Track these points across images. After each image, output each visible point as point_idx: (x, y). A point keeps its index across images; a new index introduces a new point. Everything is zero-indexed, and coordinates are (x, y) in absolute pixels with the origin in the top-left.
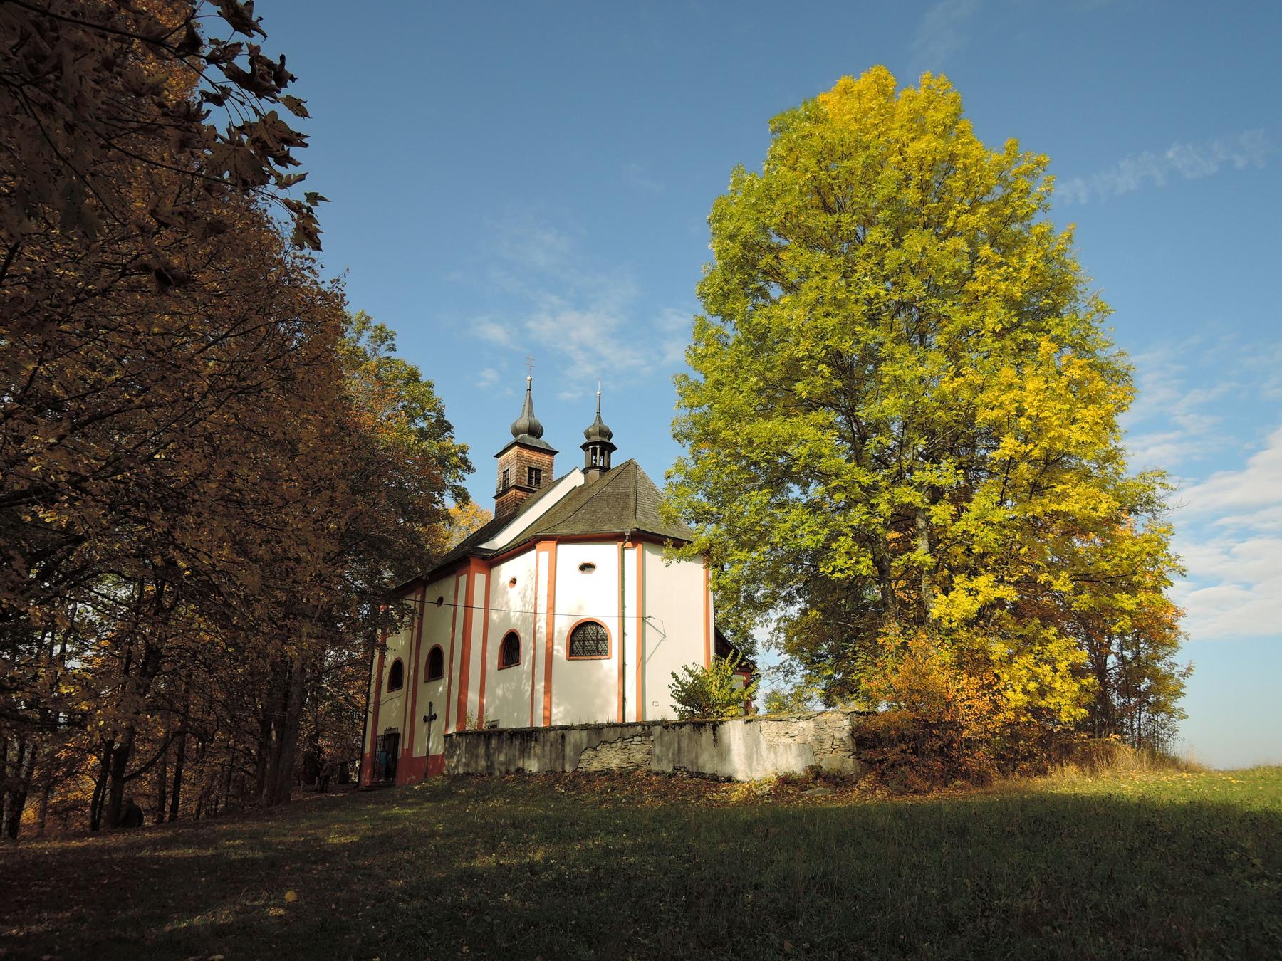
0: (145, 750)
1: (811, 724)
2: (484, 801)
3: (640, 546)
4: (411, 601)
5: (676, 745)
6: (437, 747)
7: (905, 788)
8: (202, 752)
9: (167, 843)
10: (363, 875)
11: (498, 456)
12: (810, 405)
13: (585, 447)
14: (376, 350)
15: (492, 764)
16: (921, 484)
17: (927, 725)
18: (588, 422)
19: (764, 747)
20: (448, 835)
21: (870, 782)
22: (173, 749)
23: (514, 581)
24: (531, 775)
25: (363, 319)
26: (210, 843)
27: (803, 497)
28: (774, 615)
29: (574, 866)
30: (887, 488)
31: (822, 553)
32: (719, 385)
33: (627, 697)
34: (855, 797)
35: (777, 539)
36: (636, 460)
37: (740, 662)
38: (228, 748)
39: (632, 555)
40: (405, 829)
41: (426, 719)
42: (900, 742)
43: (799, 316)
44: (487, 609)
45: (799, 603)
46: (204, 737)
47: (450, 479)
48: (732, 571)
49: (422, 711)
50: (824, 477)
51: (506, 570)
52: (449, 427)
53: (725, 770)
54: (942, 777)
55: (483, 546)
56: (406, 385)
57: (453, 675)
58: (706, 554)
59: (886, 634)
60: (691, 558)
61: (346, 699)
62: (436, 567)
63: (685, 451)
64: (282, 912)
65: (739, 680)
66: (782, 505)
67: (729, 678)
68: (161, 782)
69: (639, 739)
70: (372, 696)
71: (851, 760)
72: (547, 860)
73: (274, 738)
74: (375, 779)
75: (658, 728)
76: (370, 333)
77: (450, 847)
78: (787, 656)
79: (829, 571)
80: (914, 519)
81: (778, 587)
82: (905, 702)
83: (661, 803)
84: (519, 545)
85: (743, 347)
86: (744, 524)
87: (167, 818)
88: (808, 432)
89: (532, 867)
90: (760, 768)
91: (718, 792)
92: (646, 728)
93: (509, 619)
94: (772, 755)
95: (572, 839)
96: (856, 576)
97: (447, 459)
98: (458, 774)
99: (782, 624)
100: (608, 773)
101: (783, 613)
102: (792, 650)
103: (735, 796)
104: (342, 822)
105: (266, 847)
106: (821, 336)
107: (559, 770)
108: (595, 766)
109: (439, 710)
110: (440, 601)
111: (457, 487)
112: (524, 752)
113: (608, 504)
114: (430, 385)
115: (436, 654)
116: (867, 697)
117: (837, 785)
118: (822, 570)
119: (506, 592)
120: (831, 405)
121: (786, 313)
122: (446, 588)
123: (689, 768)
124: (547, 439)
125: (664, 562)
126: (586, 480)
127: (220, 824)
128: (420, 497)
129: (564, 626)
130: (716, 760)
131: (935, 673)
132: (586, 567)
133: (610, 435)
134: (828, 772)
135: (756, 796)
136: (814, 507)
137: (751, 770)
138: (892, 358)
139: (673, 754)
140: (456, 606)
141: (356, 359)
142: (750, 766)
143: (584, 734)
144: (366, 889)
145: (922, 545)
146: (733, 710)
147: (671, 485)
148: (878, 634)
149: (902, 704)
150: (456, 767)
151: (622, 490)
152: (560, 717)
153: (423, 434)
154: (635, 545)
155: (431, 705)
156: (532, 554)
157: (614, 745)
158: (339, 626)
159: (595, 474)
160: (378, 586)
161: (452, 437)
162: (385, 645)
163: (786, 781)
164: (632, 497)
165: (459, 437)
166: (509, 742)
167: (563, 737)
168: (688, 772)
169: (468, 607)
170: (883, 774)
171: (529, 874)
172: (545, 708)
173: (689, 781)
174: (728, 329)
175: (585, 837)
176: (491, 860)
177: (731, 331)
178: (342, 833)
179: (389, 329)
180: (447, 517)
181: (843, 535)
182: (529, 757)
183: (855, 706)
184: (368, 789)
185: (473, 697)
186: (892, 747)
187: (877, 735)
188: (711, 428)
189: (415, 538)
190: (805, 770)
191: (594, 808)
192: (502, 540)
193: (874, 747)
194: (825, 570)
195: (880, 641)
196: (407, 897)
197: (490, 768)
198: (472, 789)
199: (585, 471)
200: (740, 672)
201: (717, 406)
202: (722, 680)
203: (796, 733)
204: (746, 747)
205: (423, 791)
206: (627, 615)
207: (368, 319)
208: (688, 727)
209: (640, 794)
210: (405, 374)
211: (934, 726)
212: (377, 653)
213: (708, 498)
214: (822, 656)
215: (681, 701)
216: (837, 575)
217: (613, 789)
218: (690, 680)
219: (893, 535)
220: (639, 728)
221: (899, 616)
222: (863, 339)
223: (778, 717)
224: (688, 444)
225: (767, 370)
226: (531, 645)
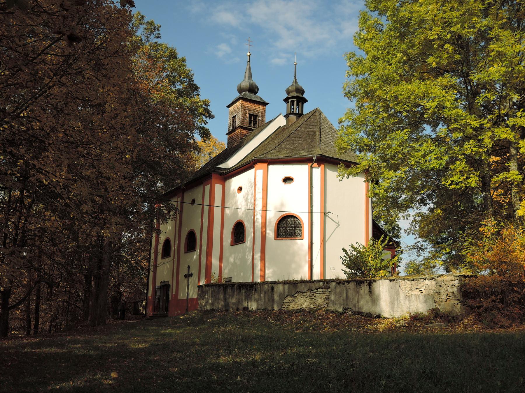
0: (18, 293)
1: (433, 283)
2: (223, 327)
3: (323, 166)
4: (175, 202)
5: (345, 294)
6: (193, 294)
7: (493, 324)
8: (51, 294)
9: (38, 345)
10: (154, 365)
11: (229, 106)
12: (438, 72)
13: (286, 100)
14: (148, 38)
15: (228, 304)
16: (514, 126)
17: (511, 284)
18: (288, 84)
19: (402, 296)
20: (203, 345)
21: (471, 320)
22: (34, 292)
23: (240, 189)
24: (252, 311)
25: (139, 17)
26: (63, 346)
27: (432, 134)
28: (412, 212)
29: (279, 363)
30: (489, 128)
31: (443, 172)
32: (375, 59)
33: (314, 264)
34: (459, 329)
35: (413, 163)
36: (321, 109)
37: (388, 242)
38: (66, 291)
39: (317, 172)
40: (176, 341)
41: (186, 276)
42: (492, 295)
43: (432, 10)
44: (223, 207)
45: (429, 204)
46: (51, 284)
47: (198, 123)
48: (384, 184)
49: (184, 271)
50: (447, 121)
51: (235, 182)
52: (197, 88)
53: (375, 310)
54: (519, 317)
55: (220, 166)
56: (168, 61)
57: (203, 248)
58: (366, 172)
59: (485, 225)
60: (356, 174)
61: (136, 263)
62: (190, 180)
63: (352, 104)
64: (110, 382)
65: (387, 255)
66: (417, 140)
67: (381, 253)
68: (28, 310)
69: (321, 290)
70: (152, 261)
71: (459, 306)
72: (262, 359)
73: (93, 286)
74: (156, 313)
75: (334, 284)
76: (144, 26)
77: (204, 351)
78: (420, 239)
79: (448, 184)
80: (509, 148)
81: (413, 194)
82: (497, 269)
83: (335, 330)
84: (243, 165)
85: (392, 33)
86: (391, 152)
87: (32, 332)
88: (437, 91)
89: (254, 363)
90: (399, 310)
91: (371, 324)
92: (326, 284)
93: (237, 214)
94: (407, 302)
95: (278, 349)
96: (467, 188)
97: (196, 109)
98: (207, 310)
99: (417, 218)
100: (301, 311)
101: (417, 211)
102: (425, 235)
103: (382, 327)
104: (138, 336)
105: (96, 348)
106: (447, 24)
107: (270, 309)
108: (293, 307)
109: (194, 271)
110: (193, 202)
111: (201, 128)
112: (248, 298)
113: (301, 138)
114: (184, 61)
115: (191, 236)
116: (471, 265)
117: (449, 321)
118: (443, 183)
119: (234, 196)
120: (453, 71)
121: (423, 9)
122: (196, 193)
123: (353, 309)
124: (261, 94)
125: (339, 178)
126: (287, 122)
127: (66, 335)
128: (179, 135)
129: (273, 218)
130: (370, 304)
131: (517, 251)
132: (287, 180)
133: (303, 92)
134: (444, 313)
135: (396, 327)
136: (439, 141)
137: (393, 311)
138: (497, 38)
139: (343, 300)
140: (203, 205)
141: (138, 45)
142: (393, 308)
143: (286, 286)
144: (156, 372)
145: (513, 166)
146: (382, 273)
147: (342, 127)
148: (481, 225)
149: (494, 270)
150: (205, 305)
151: (311, 129)
152: (270, 277)
153: (180, 93)
154: (319, 166)
155: (189, 267)
156: (252, 171)
157: (305, 294)
158: (131, 217)
159: (293, 118)
160: (154, 192)
161: (199, 95)
162: (159, 230)
163: (416, 318)
164: (318, 133)
165: (203, 95)
166: (238, 291)
167: (273, 288)
168: (352, 311)
169: (211, 206)
170: (480, 315)
171: (252, 366)
172: (261, 270)
173: (353, 317)
174: (383, 20)
175: (286, 348)
176: (230, 359)
177: (385, 22)
178: (138, 342)
179: (156, 23)
180: (197, 148)
181: (459, 160)
182: (251, 301)
183: (464, 271)
184: (151, 318)
185: (215, 262)
186: (487, 298)
187: (477, 291)
188: (369, 89)
189: (176, 160)
190: (428, 312)
191: (292, 332)
192: (232, 162)
193: (475, 298)
194: (445, 182)
195: (481, 229)
196: (181, 377)
197: (227, 305)
198: (215, 319)
199: (286, 116)
200: (388, 249)
201: (374, 74)
202: (376, 254)
203: (423, 288)
204: (390, 296)
205: (185, 320)
206: (314, 211)
207: (143, 17)
208: (352, 283)
209: (321, 324)
210: (167, 54)
211: (515, 285)
212: (154, 235)
213: (368, 136)
214: (443, 239)
215: (348, 266)
216: (453, 186)
217: (305, 321)
218: (355, 253)
219: (493, 158)
220: (321, 283)
221: (496, 213)
222: (478, 26)
223: (412, 278)
224: (354, 99)
225: (409, 48)
226: (252, 230)
